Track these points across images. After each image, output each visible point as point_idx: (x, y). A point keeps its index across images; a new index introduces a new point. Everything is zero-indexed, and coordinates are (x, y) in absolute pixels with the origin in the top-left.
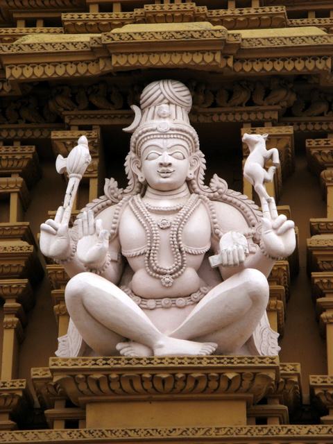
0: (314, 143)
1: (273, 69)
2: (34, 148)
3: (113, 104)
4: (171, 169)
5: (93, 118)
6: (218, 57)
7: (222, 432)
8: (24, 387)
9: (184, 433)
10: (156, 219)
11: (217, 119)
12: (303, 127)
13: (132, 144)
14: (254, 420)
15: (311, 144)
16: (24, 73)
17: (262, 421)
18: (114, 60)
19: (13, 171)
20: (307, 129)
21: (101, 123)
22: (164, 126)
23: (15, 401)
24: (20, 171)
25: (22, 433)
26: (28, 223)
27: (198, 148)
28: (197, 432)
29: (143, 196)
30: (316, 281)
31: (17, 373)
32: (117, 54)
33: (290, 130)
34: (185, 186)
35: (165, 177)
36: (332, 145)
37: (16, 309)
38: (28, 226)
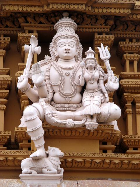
0: (122, 43)
1: (27, 10)
2: (9, 39)
3: (36, 21)
4: (69, 51)
5: (28, 27)
6: (84, 6)
7: (84, 154)
8: (10, 135)
9: (94, 155)
10: (65, 72)
11: (91, 30)
12: (119, 36)
13: (53, 39)
14: (102, 151)
15: (121, 44)
16: (19, 9)
17: (105, 151)
18: (51, 6)
19: (135, 52)
20: (120, 36)
21: (28, 29)
22: (66, 37)
23: (6, 140)
24: (3, 48)
25: (18, 152)
26: (9, 69)
27: (79, 42)
28: (82, 154)
29: (57, 62)
30: (125, 97)
31: (5, 128)
32: (52, 4)
33: (112, 37)
34: (74, 59)
35: (67, 54)
36: (139, 44)
37: (6, 102)
38: (9, 70)
